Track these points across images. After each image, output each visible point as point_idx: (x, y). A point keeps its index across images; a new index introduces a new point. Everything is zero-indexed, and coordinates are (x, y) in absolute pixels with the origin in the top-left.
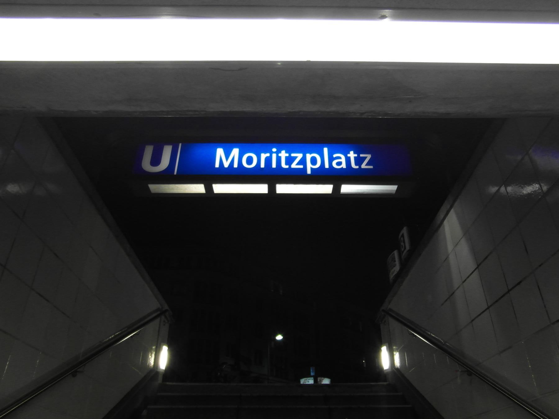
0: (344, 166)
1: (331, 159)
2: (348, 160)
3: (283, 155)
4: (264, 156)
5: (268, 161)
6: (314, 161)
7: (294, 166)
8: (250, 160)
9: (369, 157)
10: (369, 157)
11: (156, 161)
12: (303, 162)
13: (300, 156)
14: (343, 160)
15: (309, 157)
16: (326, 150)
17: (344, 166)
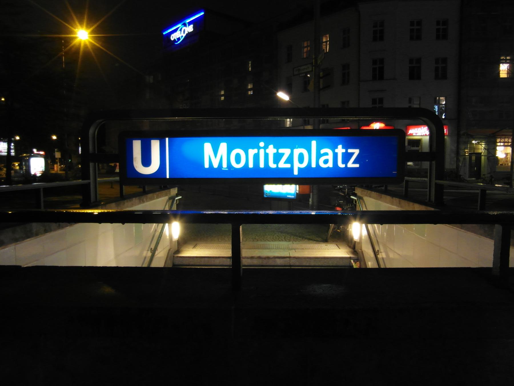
0: (330, 165)
1: (319, 156)
2: (335, 156)
3: (271, 150)
4: (252, 152)
5: (256, 157)
6: (301, 159)
7: (350, 165)
8: (238, 159)
9: (356, 152)
10: (356, 152)
11: (146, 161)
12: (290, 160)
13: (286, 152)
14: (330, 157)
15: (297, 152)
16: (314, 143)
17: (330, 165)
